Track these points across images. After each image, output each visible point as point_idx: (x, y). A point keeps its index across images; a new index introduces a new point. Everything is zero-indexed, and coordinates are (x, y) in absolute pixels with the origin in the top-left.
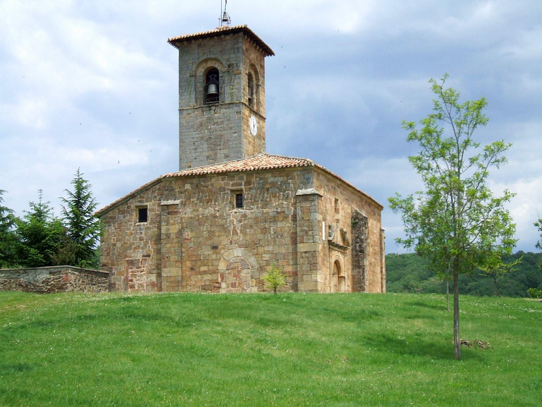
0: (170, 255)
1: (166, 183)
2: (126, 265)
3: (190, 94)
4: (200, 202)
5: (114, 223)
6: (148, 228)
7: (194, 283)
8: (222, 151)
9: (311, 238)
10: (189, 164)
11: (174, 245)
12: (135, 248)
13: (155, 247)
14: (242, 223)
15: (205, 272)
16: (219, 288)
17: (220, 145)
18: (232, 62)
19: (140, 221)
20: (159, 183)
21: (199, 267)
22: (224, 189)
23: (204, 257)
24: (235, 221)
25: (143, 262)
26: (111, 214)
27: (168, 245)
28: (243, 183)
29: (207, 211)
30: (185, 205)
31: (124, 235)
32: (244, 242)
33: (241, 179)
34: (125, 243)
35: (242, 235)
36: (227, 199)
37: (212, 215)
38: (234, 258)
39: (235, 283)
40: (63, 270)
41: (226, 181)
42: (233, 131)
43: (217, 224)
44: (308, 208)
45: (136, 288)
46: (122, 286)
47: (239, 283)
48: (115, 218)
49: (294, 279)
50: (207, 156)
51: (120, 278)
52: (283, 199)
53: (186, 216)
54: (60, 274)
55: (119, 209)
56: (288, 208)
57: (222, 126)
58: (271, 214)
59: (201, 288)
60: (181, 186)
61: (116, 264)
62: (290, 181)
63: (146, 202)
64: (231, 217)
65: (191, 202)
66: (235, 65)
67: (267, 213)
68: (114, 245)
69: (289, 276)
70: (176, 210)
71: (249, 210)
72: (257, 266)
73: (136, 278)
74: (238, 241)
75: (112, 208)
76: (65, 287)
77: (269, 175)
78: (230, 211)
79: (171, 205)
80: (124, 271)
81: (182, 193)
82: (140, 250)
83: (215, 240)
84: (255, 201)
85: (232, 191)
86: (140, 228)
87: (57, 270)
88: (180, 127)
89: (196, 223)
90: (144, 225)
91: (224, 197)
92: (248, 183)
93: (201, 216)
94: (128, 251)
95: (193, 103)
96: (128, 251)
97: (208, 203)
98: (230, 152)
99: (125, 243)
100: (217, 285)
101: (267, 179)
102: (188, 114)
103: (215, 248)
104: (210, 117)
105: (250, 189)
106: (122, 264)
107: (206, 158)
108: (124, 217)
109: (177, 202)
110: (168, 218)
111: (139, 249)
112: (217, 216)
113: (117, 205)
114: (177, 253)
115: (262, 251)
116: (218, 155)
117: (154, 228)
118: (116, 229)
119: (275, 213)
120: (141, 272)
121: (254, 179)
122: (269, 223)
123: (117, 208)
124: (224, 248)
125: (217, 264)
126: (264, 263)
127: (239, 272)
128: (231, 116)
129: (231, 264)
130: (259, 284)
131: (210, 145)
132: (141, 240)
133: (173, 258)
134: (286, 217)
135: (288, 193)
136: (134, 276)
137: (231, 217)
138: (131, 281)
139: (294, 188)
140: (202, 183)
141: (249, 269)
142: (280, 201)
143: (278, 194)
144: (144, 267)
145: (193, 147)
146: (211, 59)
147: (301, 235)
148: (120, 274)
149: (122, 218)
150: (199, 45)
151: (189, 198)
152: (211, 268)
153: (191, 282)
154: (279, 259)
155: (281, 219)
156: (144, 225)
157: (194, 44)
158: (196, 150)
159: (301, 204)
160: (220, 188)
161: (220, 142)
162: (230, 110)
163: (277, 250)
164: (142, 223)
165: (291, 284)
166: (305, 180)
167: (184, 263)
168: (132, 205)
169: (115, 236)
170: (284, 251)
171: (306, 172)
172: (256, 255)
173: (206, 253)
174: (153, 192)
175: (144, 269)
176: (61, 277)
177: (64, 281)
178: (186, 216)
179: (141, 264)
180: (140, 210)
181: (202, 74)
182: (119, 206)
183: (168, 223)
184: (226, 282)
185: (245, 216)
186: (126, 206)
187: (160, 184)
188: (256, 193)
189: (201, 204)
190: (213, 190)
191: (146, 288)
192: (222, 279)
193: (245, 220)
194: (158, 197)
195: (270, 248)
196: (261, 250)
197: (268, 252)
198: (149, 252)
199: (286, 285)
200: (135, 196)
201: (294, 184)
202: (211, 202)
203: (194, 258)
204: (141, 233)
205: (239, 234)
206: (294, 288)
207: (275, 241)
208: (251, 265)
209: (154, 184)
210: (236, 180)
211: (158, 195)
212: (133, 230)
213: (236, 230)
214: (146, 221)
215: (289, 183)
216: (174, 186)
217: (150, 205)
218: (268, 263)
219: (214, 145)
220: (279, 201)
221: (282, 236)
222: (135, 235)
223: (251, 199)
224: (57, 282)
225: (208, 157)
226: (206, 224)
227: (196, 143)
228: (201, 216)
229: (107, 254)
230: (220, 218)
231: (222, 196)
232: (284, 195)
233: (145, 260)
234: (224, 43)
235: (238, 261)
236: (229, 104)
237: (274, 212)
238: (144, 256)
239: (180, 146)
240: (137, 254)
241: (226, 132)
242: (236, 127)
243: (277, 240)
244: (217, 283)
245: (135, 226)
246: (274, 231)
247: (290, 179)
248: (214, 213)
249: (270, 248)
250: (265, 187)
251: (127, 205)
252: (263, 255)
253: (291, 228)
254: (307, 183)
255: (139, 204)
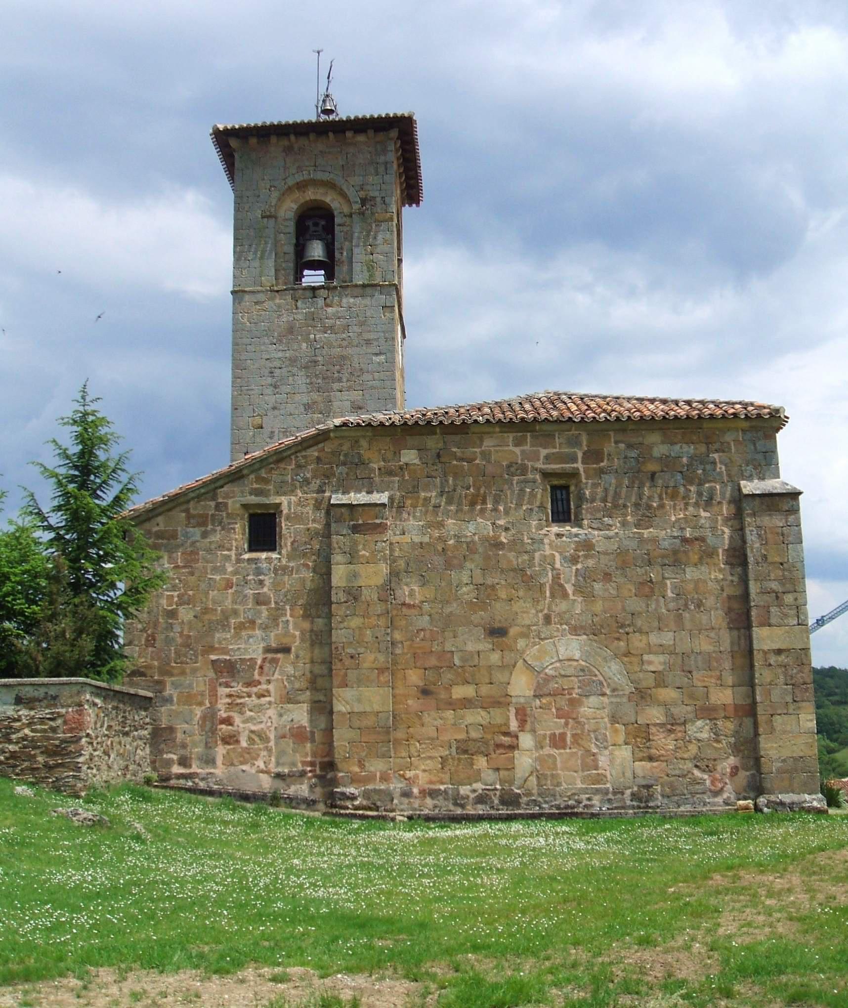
0: (361, 650)
1: (341, 445)
2: (211, 674)
3: (262, 258)
4: (449, 502)
5: (171, 551)
6: (284, 569)
7: (435, 735)
8: (345, 395)
9: (793, 612)
10: (258, 420)
11: (373, 621)
12: (241, 627)
13: (306, 625)
14: (579, 566)
15: (466, 703)
16: (513, 747)
17: (340, 380)
18: (372, 194)
19: (251, 549)
20: (317, 444)
21: (448, 689)
22: (523, 470)
23: (462, 659)
24: (558, 557)
25: (266, 669)
26: (160, 524)
27: (355, 622)
28: (580, 455)
29: (472, 527)
30: (401, 507)
31: (203, 586)
32: (587, 619)
33: (574, 442)
34: (206, 611)
35: (580, 599)
36: (533, 495)
37: (485, 539)
38: (558, 665)
39: (563, 736)
40: (66, 692)
41: (527, 448)
42: (377, 350)
43: (504, 564)
44: (779, 530)
45: (244, 744)
46: (197, 738)
47: (573, 736)
48: (174, 536)
49: (740, 725)
50: (304, 405)
51: (191, 711)
52: (697, 505)
53: (406, 539)
54: (55, 706)
55: (187, 511)
56: (714, 528)
57: (344, 336)
58: (666, 544)
59: (454, 749)
60: (389, 455)
61: (175, 671)
62: (716, 456)
63: (278, 493)
64: (547, 547)
65: (421, 502)
66: (379, 199)
67: (655, 540)
68: (172, 614)
69: (726, 717)
70: (378, 521)
71: (600, 530)
72: (629, 688)
73: (241, 713)
74: (567, 616)
75: (166, 507)
76: (72, 748)
77: (653, 438)
78: (543, 532)
79: (364, 505)
80: (202, 694)
81: (390, 473)
82: (258, 632)
83: (499, 611)
84: (615, 506)
85: (546, 475)
86: (257, 568)
87: (42, 690)
88: (235, 331)
89: (438, 560)
90: (269, 560)
91: (522, 490)
92: (593, 456)
93: (451, 542)
94: (217, 635)
95: (268, 279)
96: (217, 635)
97: (473, 504)
98: (367, 396)
99: (206, 611)
100: (506, 740)
101: (650, 448)
102: (256, 303)
103: (497, 632)
104: (313, 313)
105: (602, 472)
106: (194, 671)
107: (302, 408)
108: (205, 535)
109: (382, 498)
110: (355, 543)
111: (254, 629)
112: (502, 543)
113: (182, 500)
114: (383, 646)
115: (642, 645)
116: (336, 404)
117: (303, 569)
118: (177, 567)
119: (677, 541)
120: (260, 696)
121: (609, 447)
122: (659, 569)
123: (184, 507)
124: (525, 635)
125: (506, 680)
126: (650, 681)
127: (573, 703)
128: (368, 314)
129: (548, 679)
130: (635, 737)
131: (314, 380)
132: (258, 603)
133: (370, 659)
134: (709, 554)
135: (712, 491)
136: (237, 708)
137: (547, 547)
138: (228, 721)
139: (729, 475)
140: (454, 450)
141: (604, 695)
142: (691, 509)
143: (682, 489)
144: (269, 682)
145: (270, 380)
146: (315, 183)
147: (762, 603)
148: (189, 699)
149: (198, 537)
150: (288, 150)
151: (415, 489)
152: (485, 690)
153: (424, 730)
154: (693, 668)
155: (695, 558)
156: (269, 560)
157: (276, 145)
158: (275, 387)
159: (758, 519)
160: (509, 466)
161: (339, 372)
162: (367, 301)
163: (685, 644)
164: (264, 555)
165: (732, 740)
166: (760, 457)
167: (400, 675)
168: (230, 502)
169: (174, 588)
170: (706, 646)
171: (760, 434)
172: (625, 655)
173: (471, 647)
174: (299, 466)
175: (271, 687)
176: (60, 715)
177: (71, 730)
178: (406, 539)
179: (261, 674)
180: (252, 516)
181: (291, 215)
182: (188, 502)
183: (352, 557)
184: (533, 731)
185: (587, 545)
186: (213, 504)
187: (321, 445)
188: (619, 485)
189: (453, 508)
190: (490, 469)
191: (276, 744)
192: (522, 723)
193: (586, 557)
194: (316, 484)
195: (667, 638)
196: (638, 642)
197: (662, 649)
198: (286, 641)
199: (718, 741)
200: (243, 477)
201: (726, 465)
202: (484, 502)
203: (433, 661)
204: (261, 582)
205: (571, 597)
206: (739, 751)
207: (679, 618)
208: (609, 685)
209: (305, 445)
210: (559, 446)
211: (315, 477)
212: (235, 573)
213: (561, 586)
214: (272, 548)
215: (714, 463)
216: (366, 455)
217: (289, 503)
218: (660, 680)
219: (324, 378)
220: (686, 509)
221: (699, 604)
222: (239, 588)
223: (604, 500)
224: (45, 731)
225: (308, 407)
226: (469, 565)
227: (277, 372)
228: (451, 542)
229: (147, 640)
230: (510, 550)
231: (516, 489)
232: (699, 494)
233: (274, 661)
234: (351, 150)
235: (569, 672)
236: (364, 286)
237: (675, 538)
238: (268, 650)
239: (235, 377)
240: (247, 642)
241: (357, 350)
242: (382, 341)
243: (686, 615)
244: (506, 734)
245: (239, 561)
246: (676, 592)
247: (717, 451)
248: (491, 533)
249: (667, 638)
250: (643, 468)
251: (214, 498)
252: (646, 657)
253: (724, 583)
254: (763, 463)
255: (253, 499)
